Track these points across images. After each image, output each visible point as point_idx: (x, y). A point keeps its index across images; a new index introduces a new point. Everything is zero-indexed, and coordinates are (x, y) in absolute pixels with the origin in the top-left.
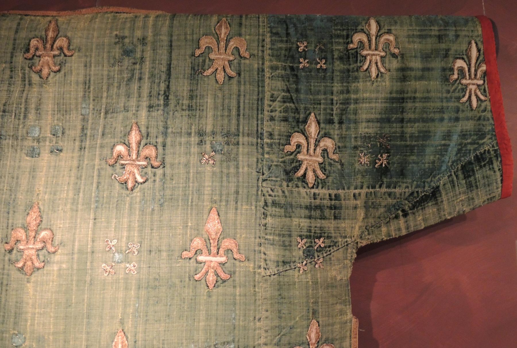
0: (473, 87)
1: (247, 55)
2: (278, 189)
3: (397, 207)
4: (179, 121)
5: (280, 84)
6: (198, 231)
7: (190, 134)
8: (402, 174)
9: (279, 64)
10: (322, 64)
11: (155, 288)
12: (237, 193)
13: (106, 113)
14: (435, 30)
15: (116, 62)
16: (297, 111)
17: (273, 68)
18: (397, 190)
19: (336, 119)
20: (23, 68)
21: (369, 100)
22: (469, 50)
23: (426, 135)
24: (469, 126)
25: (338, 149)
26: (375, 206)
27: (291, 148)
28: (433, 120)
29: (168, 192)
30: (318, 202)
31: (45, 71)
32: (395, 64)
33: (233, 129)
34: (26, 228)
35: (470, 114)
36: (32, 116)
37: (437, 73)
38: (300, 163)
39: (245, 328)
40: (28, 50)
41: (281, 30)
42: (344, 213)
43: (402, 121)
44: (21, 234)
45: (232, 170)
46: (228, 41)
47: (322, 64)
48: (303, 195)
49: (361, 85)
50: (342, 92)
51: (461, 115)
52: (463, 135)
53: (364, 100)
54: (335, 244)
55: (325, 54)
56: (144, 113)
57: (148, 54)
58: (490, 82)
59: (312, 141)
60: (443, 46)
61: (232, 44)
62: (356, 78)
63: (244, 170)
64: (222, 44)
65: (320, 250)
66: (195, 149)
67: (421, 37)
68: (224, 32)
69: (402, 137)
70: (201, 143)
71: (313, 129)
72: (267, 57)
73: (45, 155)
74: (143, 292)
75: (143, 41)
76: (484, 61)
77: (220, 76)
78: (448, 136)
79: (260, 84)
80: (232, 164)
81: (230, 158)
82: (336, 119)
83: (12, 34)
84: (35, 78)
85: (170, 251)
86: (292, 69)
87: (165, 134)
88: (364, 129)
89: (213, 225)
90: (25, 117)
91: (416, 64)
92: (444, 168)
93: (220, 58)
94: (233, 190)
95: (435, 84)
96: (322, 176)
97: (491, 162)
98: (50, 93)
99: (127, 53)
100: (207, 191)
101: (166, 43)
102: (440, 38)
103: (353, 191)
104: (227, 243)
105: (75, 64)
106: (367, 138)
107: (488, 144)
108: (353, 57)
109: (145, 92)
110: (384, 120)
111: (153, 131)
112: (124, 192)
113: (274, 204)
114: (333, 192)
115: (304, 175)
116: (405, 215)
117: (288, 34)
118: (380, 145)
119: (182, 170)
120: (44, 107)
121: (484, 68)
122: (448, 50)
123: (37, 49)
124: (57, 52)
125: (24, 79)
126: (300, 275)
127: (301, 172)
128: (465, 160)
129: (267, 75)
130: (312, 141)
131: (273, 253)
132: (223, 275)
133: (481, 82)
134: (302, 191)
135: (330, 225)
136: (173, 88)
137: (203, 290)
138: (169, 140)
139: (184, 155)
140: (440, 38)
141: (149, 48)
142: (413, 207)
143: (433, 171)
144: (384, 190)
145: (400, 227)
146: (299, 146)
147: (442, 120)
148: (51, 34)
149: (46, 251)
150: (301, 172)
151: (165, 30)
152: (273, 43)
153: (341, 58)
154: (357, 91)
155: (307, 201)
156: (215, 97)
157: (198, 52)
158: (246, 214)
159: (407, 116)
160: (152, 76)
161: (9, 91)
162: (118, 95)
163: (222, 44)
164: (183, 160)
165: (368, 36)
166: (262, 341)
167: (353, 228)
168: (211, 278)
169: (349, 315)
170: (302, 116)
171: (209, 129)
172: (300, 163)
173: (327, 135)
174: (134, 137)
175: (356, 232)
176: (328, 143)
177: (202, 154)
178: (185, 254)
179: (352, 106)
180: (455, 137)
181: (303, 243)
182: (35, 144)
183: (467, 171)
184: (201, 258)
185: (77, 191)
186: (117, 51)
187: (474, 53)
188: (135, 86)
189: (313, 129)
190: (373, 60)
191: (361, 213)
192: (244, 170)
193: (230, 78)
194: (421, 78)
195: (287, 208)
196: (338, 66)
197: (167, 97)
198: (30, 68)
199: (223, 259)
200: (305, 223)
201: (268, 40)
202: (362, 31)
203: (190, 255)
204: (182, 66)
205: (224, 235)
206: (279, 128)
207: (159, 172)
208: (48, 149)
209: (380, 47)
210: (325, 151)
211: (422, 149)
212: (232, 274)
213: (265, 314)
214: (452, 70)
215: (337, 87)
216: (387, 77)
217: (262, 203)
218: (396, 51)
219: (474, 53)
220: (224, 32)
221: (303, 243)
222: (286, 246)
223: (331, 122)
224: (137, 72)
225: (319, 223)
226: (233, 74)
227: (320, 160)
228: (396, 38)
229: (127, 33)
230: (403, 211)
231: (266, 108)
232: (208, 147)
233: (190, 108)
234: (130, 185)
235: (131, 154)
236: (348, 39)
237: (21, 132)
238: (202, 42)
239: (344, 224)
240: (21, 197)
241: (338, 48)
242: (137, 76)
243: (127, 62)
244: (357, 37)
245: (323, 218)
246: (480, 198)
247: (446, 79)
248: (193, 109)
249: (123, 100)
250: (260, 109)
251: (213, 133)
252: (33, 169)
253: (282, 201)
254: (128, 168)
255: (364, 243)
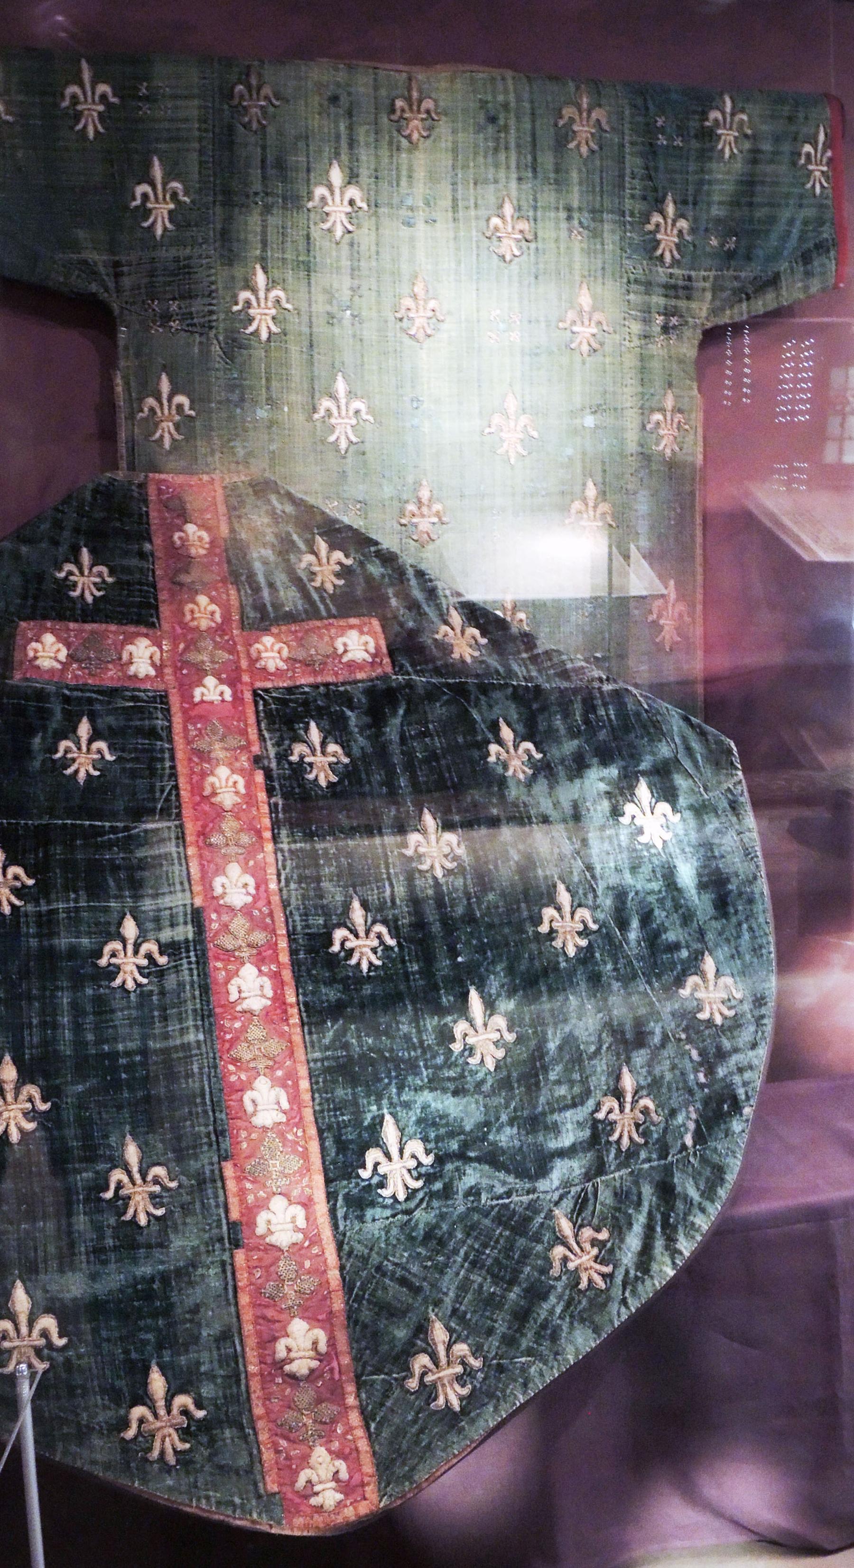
0: (817, 174)
1: (607, 128)
2: (638, 267)
3: (741, 290)
4: (548, 196)
5: (639, 161)
6: (572, 303)
7: (557, 209)
8: (749, 258)
9: (640, 140)
10: (678, 142)
11: (537, 355)
12: (603, 268)
13: (475, 184)
14: (786, 110)
15: (480, 129)
16: (655, 190)
17: (632, 143)
18: (743, 274)
19: (690, 199)
20: (390, 132)
21: (722, 182)
22: (816, 134)
23: (772, 220)
24: (809, 212)
25: (693, 231)
26: (722, 289)
27: (650, 227)
28: (779, 205)
29: (541, 266)
30: (673, 281)
31: (415, 136)
32: (747, 145)
33: (597, 206)
34: (415, 297)
35: (812, 201)
36: (404, 182)
37: (786, 158)
38: (658, 242)
39: (614, 393)
40: (393, 111)
41: (639, 101)
42: (695, 294)
43: (751, 204)
44: (408, 302)
45: (599, 247)
46: (589, 112)
47: (678, 142)
48: (661, 274)
49: (714, 166)
50: (696, 173)
51: (805, 202)
52: (805, 223)
53: (718, 182)
54: (687, 322)
55: (681, 131)
56: (513, 184)
57: (512, 122)
58: (834, 170)
59: (670, 221)
60: (793, 128)
61: (594, 115)
62: (710, 159)
63: (609, 247)
64: (585, 115)
65: (674, 327)
66: (564, 225)
67: (772, 117)
68: (585, 102)
69: (751, 221)
70: (569, 218)
71: (670, 209)
72: (627, 131)
73: (421, 226)
74: (527, 359)
75: (506, 106)
76: (830, 147)
77: (584, 150)
78: (791, 222)
79: (621, 161)
80: (598, 240)
81: (596, 234)
82: (690, 199)
83: (371, 91)
84: (404, 143)
85: (548, 323)
86: (651, 144)
87: (535, 208)
88: (716, 211)
89: (585, 300)
90: (398, 185)
91: (767, 147)
92: (786, 253)
93: (584, 130)
94: (600, 265)
95: (783, 169)
96: (677, 256)
97: (828, 251)
98: (420, 160)
99: (493, 120)
100: (577, 266)
101: (529, 111)
102: (790, 119)
103: (703, 273)
104: (597, 316)
105: (443, 128)
106: (718, 221)
107: (826, 233)
108: (708, 135)
109: (513, 164)
110: (734, 203)
111: (524, 203)
112: (502, 264)
113: (636, 281)
114: (686, 273)
115: (662, 255)
116: (748, 298)
117: (647, 109)
118: (727, 228)
119: (553, 245)
120: (415, 175)
121: (829, 154)
122: (797, 133)
123: (403, 110)
124: (424, 116)
125: (390, 143)
126: (658, 347)
127: (659, 252)
128: (805, 246)
129: (627, 150)
130: (670, 221)
131: (636, 328)
132: (595, 345)
133: (825, 169)
134: (660, 270)
135: (682, 304)
136: (539, 160)
137: (578, 358)
138: (539, 213)
139: (553, 229)
140: (790, 119)
141: (512, 115)
142: (756, 291)
143: (775, 256)
144: (731, 273)
145: (741, 312)
146: (658, 225)
147: (787, 205)
148: (415, 94)
149: (435, 317)
150: (659, 252)
151: (526, 96)
152: (632, 116)
153: (696, 136)
154: (710, 172)
155: (663, 279)
156: (580, 171)
157: (561, 123)
158: (611, 290)
159: (758, 199)
160: (518, 146)
161: (377, 156)
162: (486, 164)
163: (585, 115)
164: (553, 235)
165: (723, 113)
166: (629, 405)
167: (701, 311)
168: (585, 348)
169: (695, 392)
170: (660, 194)
171: (575, 204)
172: (658, 242)
173: (683, 216)
174: (508, 210)
175: (704, 314)
176: (683, 224)
177: (570, 231)
178: (561, 325)
179: (706, 187)
180: (798, 223)
181: (660, 320)
182: (410, 213)
183: (806, 258)
184: (575, 329)
185: (459, 262)
186: (481, 118)
187: (822, 137)
188: (502, 156)
189: (670, 209)
190: (728, 141)
191: (709, 295)
192: (609, 247)
193: (593, 152)
194: (772, 161)
195: (648, 286)
196: (695, 144)
197: (534, 170)
198: (399, 131)
199: (594, 330)
200: (662, 301)
201: (627, 112)
202: (718, 108)
203: (566, 325)
204: (546, 138)
205: (594, 309)
206: (639, 206)
207: (533, 245)
208: (422, 219)
209: (735, 126)
210: (680, 232)
211: (767, 232)
212: (602, 344)
213: (630, 381)
214: (800, 155)
215: (692, 167)
216: (739, 159)
217: (625, 280)
218: (749, 132)
219: (822, 137)
220: (585, 102)
221: (660, 320)
222: (646, 321)
223: (685, 202)
224: (502, 141)
225: (673, 302)
226: (595, 147)
227: (676, 240)
228: (750, 117)
229: (490, 98)
230: (747, 294)
231: (627, 185)
232: (576, 222)
233: (557, 182)
234: (508, 258)
235: (509, 226)
236: (704, 116)
237: (395, 201)
238: (564, 112)
239: (694, 305)
240: (405, 267)
241: (694, 124)
242: (502, 146)
243: (490, 129)
244: (715, 115)
245: (677, 297)
246: (815, 286)
247: (794, 164)
248: (560, 183)
249: (492, 170)
250: (622, 187)
251: (580, 209)
252: (412, 239)
253: (643, 278)
254: (505, 241)
255: (709, 325)
